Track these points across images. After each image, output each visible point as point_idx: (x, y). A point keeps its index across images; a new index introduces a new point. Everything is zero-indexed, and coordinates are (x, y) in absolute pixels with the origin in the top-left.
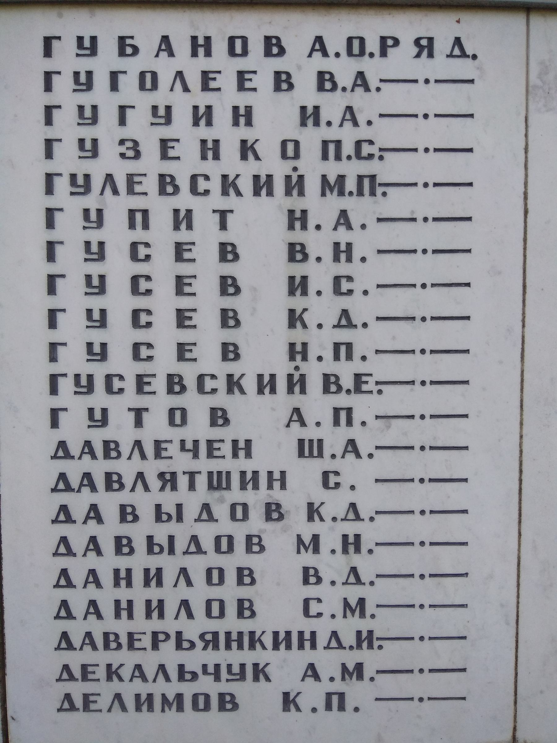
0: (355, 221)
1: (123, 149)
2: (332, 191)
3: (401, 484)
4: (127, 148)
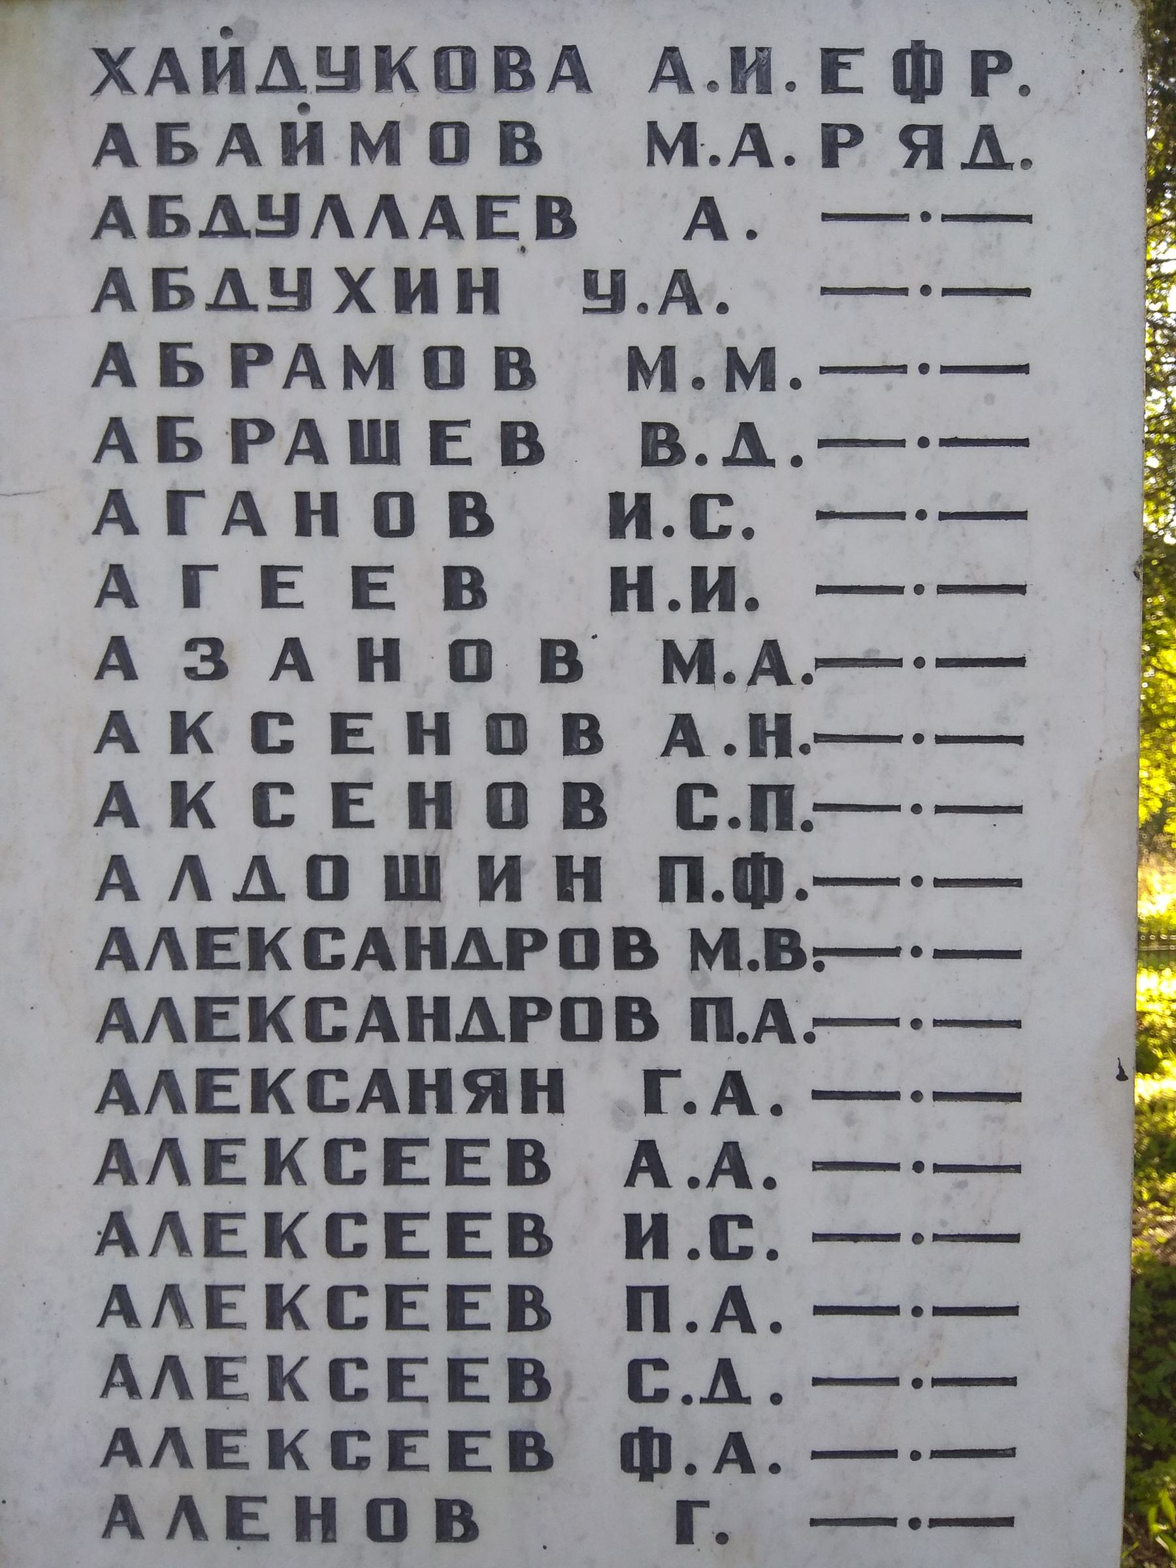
0: (760, 1099)
1: (192, 659)
2: (747, 382)
3: (984, 1031)
4: (204, 658)
